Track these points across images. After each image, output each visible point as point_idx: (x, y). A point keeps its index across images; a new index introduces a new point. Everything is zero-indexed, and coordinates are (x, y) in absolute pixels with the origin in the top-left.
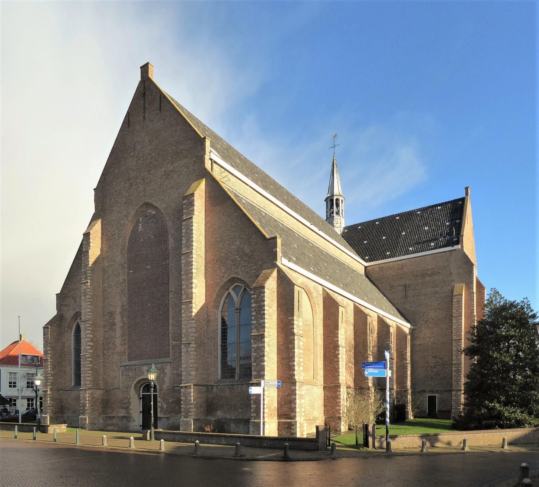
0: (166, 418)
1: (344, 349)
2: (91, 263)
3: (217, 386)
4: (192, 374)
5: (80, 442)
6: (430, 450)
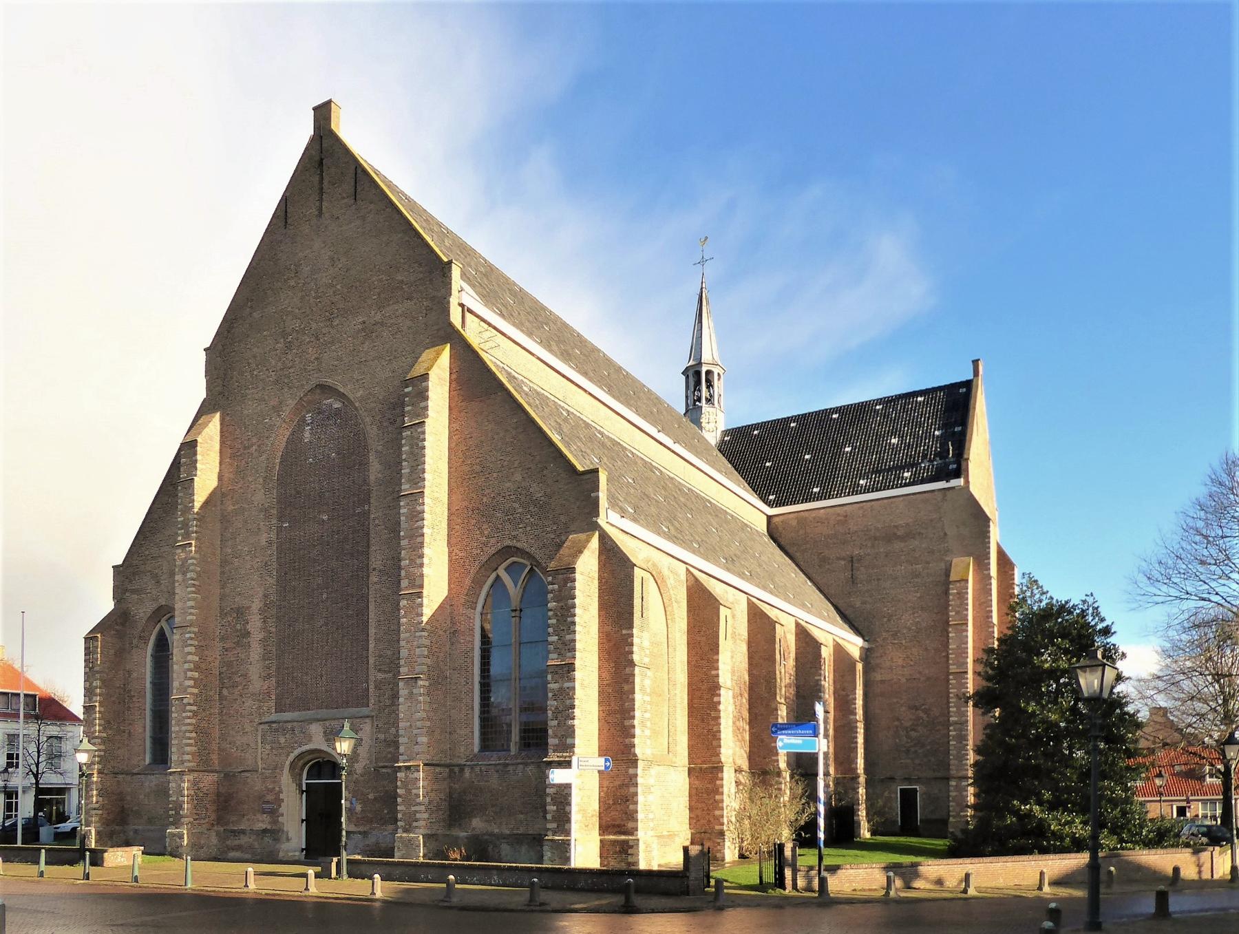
0: (360, 833)
1: (730, 693)
2: (197, 505)
3: (472, 767)
4: (422, 739)
5: (194, 880)
6: (903, 895)
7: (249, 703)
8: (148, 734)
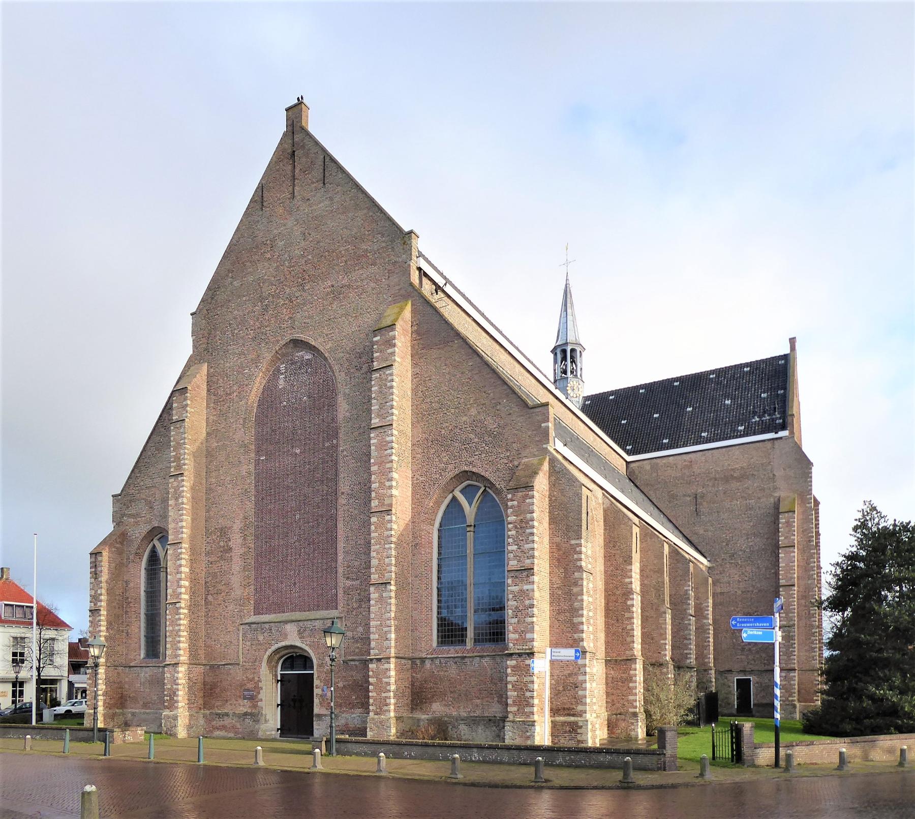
3: (432, 659)
7: (231, 607)
8: (143, 633)
